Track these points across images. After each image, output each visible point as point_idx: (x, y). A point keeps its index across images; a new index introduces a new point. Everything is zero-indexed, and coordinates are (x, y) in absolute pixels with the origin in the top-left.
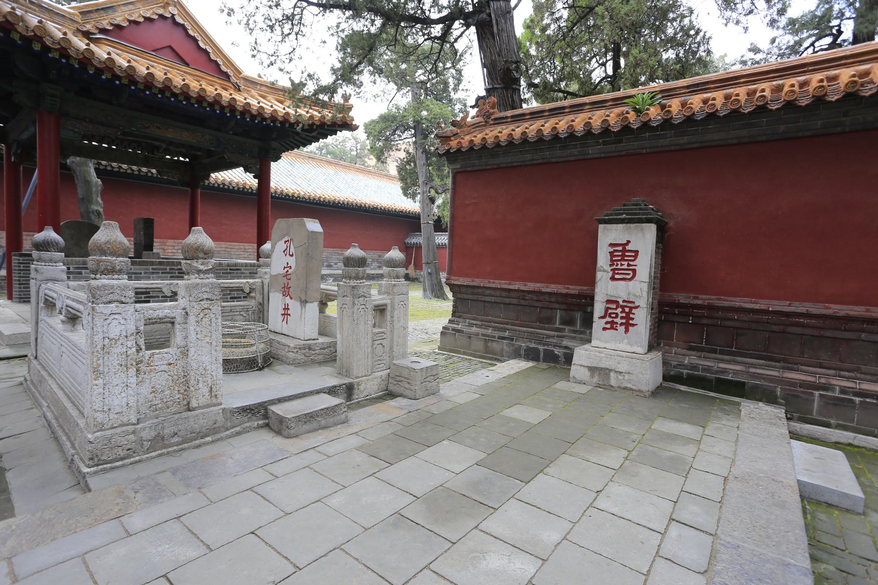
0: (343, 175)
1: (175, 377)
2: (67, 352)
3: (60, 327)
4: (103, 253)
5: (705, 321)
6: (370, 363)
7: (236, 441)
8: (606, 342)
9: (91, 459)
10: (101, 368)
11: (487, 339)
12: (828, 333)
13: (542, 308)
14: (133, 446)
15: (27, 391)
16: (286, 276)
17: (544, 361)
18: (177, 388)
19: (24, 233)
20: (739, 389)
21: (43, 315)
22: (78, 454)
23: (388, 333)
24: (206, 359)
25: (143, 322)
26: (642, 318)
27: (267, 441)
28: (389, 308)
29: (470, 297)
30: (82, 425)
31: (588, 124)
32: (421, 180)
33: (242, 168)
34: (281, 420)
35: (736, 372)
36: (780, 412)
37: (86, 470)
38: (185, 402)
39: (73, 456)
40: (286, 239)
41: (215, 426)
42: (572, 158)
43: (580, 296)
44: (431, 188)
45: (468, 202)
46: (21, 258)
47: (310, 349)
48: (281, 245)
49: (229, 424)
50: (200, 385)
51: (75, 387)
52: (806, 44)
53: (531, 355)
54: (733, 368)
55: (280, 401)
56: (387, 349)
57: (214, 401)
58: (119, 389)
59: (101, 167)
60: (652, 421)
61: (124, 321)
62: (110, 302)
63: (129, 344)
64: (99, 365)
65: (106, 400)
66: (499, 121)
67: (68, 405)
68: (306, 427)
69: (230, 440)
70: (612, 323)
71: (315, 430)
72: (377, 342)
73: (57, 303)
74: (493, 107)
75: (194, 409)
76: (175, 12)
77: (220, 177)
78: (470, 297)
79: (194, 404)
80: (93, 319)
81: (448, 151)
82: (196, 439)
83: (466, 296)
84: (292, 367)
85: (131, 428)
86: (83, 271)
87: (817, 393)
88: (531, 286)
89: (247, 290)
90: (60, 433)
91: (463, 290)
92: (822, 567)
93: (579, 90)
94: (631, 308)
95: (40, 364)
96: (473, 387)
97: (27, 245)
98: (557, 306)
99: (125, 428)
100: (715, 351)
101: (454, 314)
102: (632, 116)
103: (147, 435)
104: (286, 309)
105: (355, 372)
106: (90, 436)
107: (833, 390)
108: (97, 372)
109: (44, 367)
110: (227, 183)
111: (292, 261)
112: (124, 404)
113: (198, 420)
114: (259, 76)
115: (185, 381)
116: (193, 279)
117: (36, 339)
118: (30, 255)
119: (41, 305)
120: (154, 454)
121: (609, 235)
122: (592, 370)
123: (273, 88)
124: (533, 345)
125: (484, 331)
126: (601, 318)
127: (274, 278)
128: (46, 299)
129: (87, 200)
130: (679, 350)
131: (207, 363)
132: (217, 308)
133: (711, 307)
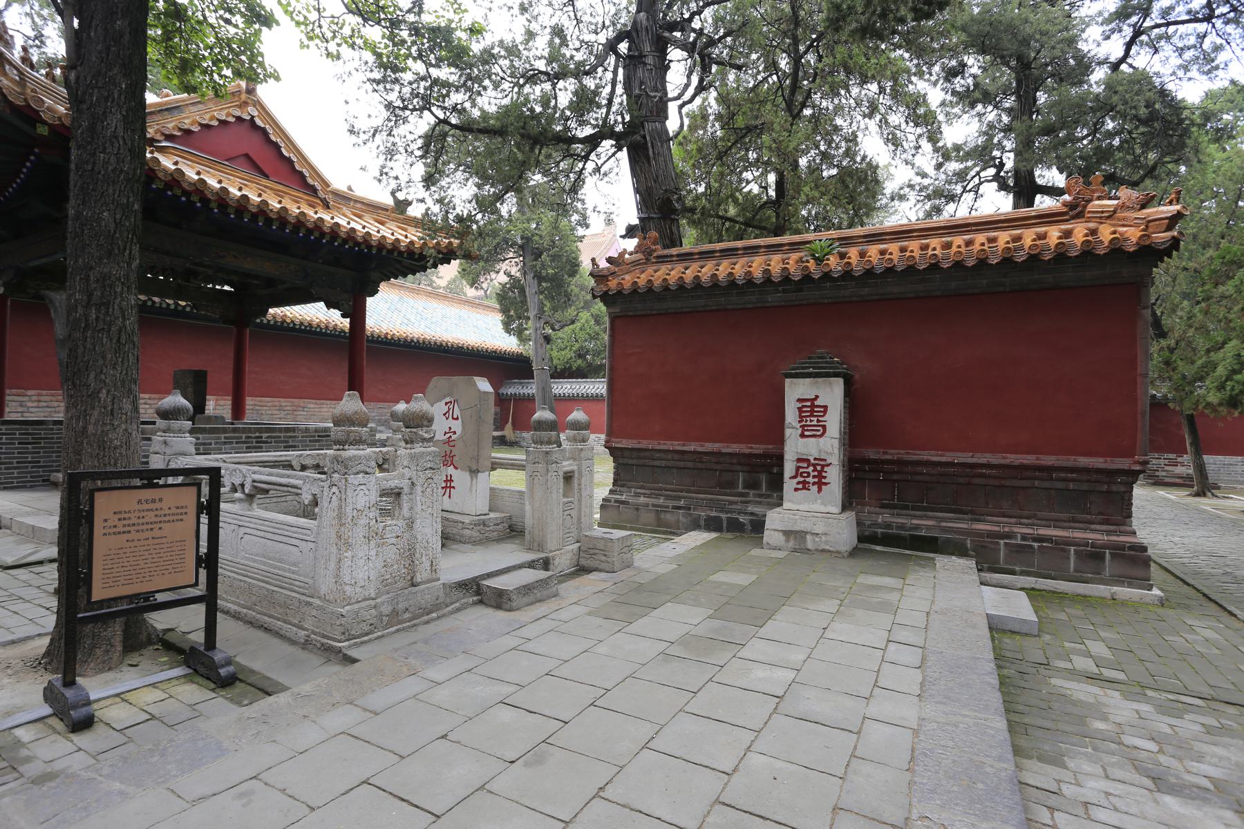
0: (412, 302)
5: (895, 477)
8: (799, 504)
12: (1008, 483)
13: (721, 471)
17: (728, 531)
19: (8, 391)
20: (929, 545)
26: (834, 475)
27: (482, 618)
29: (635, 462)
31: (766, 271)
34: (500, 593)
35: (928, 528)
36: (972, 563)
40: (448, 400)
42: (750, 306)
43: (765, 456)
47: (484, 525)
52: (973, 173)
53: (712, 525)
54: (925, 524)
55: (490, 575)
56: (575, 521)
60: (856, 577)
66: (662, 259)
68: (526, 600)
70: (804, 483)
71: (532, 603)
74: (655, 243)
76: (256, 114)
78: (635, 462)
79: (418, 579)
81: (606, 293)
84: (469, 546)
85: (372, 603)
87: (1002, 542)
88: (710, 447)
91: (627, 454)
92: (1005, 671)
93: (738, 215)
94: (823, 466)
98: (739, 468)
100: (906, 508)
101: (615, 483)
102: (812, 265)
103: (386, 609)
104: (449, 480)
107: (1016, 538)
111: (457, 426)
113: (425, 595)
114: (350, 189)
115: (410, 554)
121: (796, 391)
122: (787, 534)
123: (373, 208)
124: (714, 514)
125: (655, 501)
126: (792, 478)
130: (872, 509)
133: (900, 462)
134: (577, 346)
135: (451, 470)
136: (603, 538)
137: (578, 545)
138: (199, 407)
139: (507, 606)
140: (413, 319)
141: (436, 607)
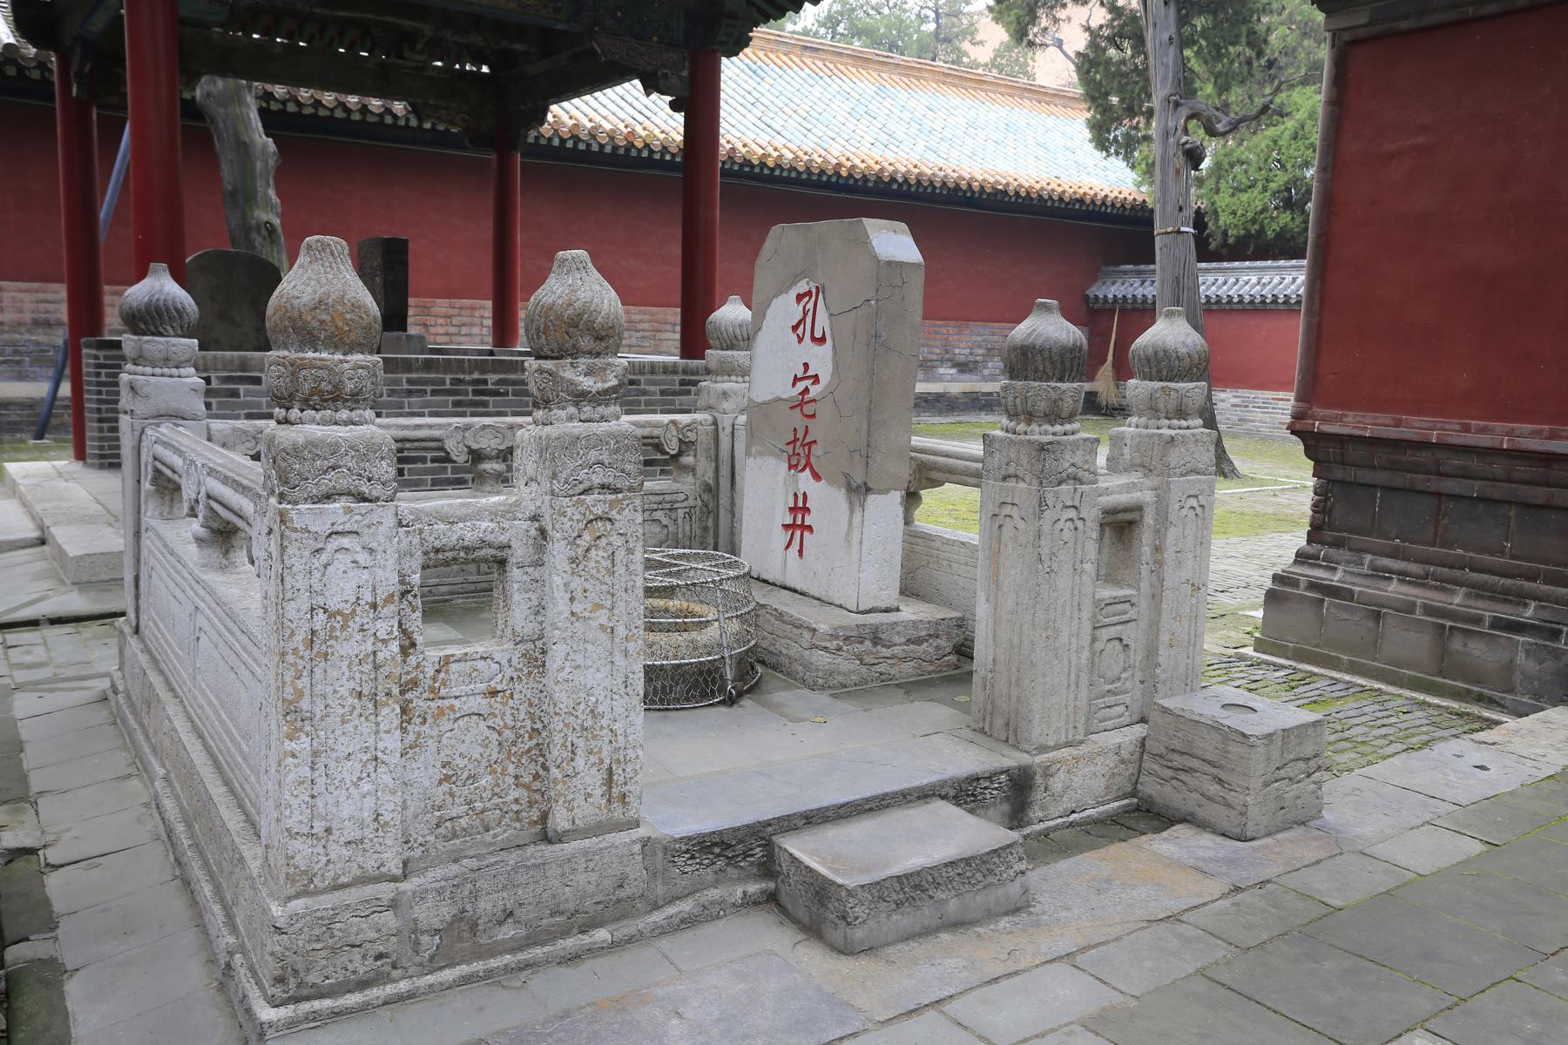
1: (508, 734)
2: (212, 633)
3: (192, 552)
4: (309, 339)
6: (1082, 703)
7: (681, 946)
9: (280, 980)
10: (305, 704)
11: (1446, 626)
14: (391, 946)
15: (116, 720)
16: (802, 404)
18: (511, 769)
19: (106, 288)
21: (150, 517)
22: (243, 950)
23: (1144, 604)
24: (597, 678)
25: (417, 560)
28: (1149, 519)
29: (1382, 477)
30: (254, 866)
32: (1160, 92)
33: (637, 82)
34: (822, 890)
37: (267, 1014)
38: (535, 814)
39: (231, 954)
40: (802, 287)
41: (622, 894)
44: (1189, 118)
45: (1389, 147)
46: (101, 354)
47: (876, 641)
48: (785, 309)
49: (660, 890)
50: (580, 762)
51: (232, 739)
55: (812, 819)
56: (1137, 656)
57: (618, 813)
58: (349, 771)
59: (274, 106)
61: (365, 554)
62: (328, 497)
63: (382, 628)
64: (300, 694)
65: (320, 802)
67: (217, 790)
68: (903, 920)
69: (664, 943)
71: (928, 932)
72: (1105, 634)
73: (183, 483)
75: (560, 838)
77: (565, 118)
78: (1382, 477)
79: (560, 820)
80: (283, 549)
82: (565, 933)
83: (1367, 476)
84: (822, 699)
86: (242, 388)
89: (672, 447)
90: (197, 872)
95: (147, 650)
96: (1444, 808)
97: (112, 319)
99: (369, 891)
103: (432, 913)
104: (800, 508)
105: (1038, 731)
106: (276, 910)
108: (295, 717)
109: (154, 661)
110: (583, 135)
111: (821, 360)
112: (367, 815)
113: (576, 872)
115: (532, 747)
116: (565, 423)
117: (137, 579)
118: (117, 345)
119: (147, 485)
120: (448, 975)
125: (1437, 598)
127: (760, 412)
128: (157, 470)
129: (244, 196)
131: (599, 693)
132: (630, 518)
134: (1281, 179)
135: (805, 480)
136: (1216, 728)
137: (1139, 730)
138: (394, 318)
139: (836, 935)
140: (900, 135)
141: (615, 908)
